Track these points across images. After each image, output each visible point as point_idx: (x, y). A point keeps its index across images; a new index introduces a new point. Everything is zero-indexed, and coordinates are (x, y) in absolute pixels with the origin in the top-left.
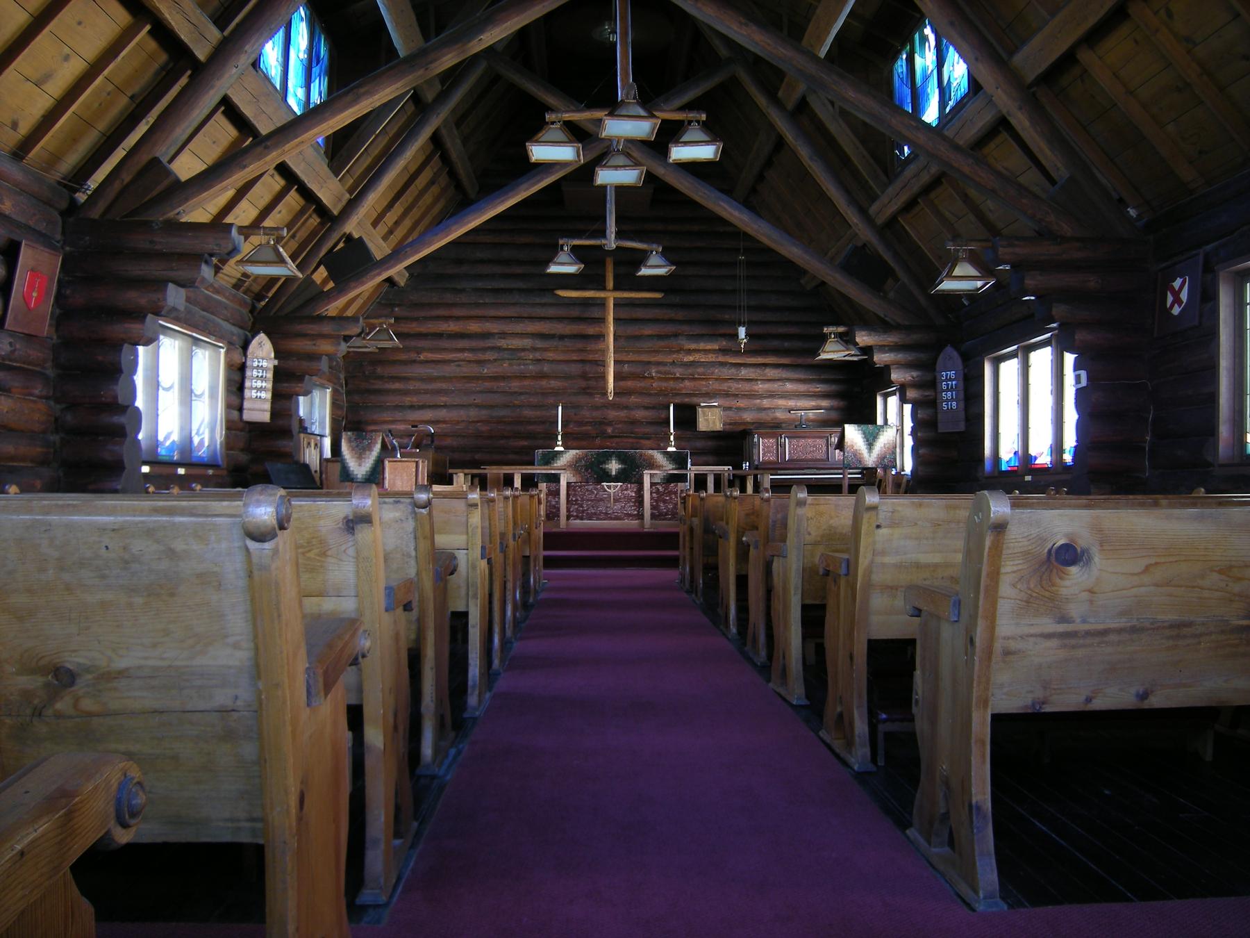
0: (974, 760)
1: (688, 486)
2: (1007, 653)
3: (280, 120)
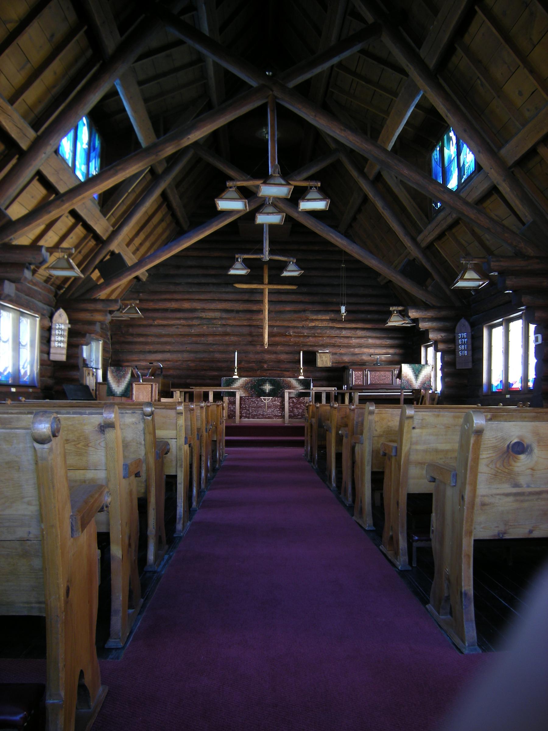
0: (464, 567)
1: (310, 400)
2: (483, 504)
3: (71, 184)
